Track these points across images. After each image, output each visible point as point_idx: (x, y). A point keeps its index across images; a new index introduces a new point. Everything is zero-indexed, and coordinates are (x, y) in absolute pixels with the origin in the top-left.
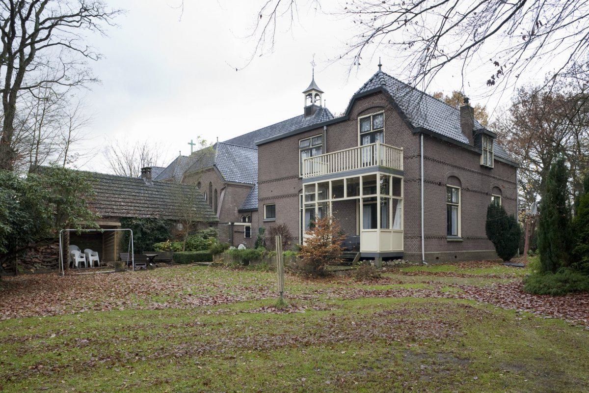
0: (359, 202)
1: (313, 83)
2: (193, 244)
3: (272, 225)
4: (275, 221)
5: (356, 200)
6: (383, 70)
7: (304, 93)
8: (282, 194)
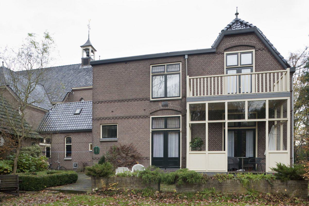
0: (225, 127)
1: (88, 41)
2: (25, 164)
3: (112, 145)
4: (116, 141)
5: (221, 123)
6: (239, 17)
7: (81, 47)
8: (127, 115)
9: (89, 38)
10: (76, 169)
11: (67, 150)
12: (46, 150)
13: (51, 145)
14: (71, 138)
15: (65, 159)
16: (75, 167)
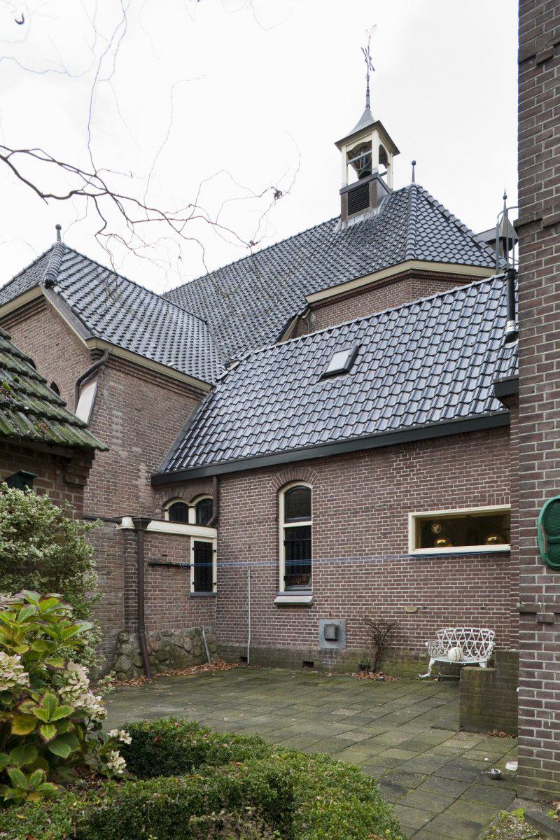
7: (339, 144)
9: (368, 106)
10: (337, 652)
11: (289, 556)
12: (192, 562)
13: (219, 533)
14: (309, 490)
15: (279, 599)
16: (328, 646)
